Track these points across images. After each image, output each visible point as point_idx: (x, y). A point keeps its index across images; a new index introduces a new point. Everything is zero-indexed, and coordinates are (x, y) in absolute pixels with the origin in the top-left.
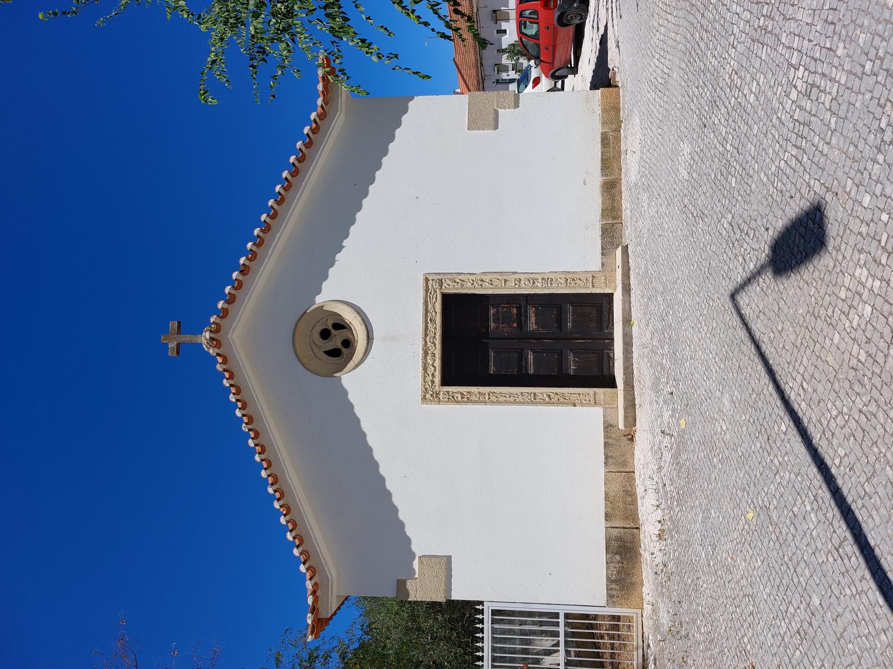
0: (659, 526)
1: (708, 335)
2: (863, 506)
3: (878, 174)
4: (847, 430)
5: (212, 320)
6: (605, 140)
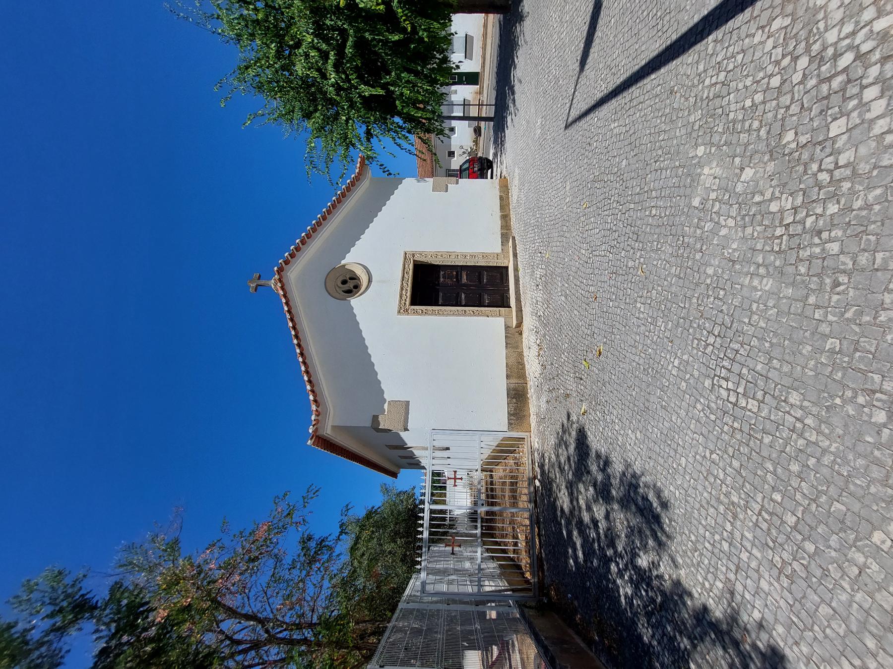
6: (501, 198)
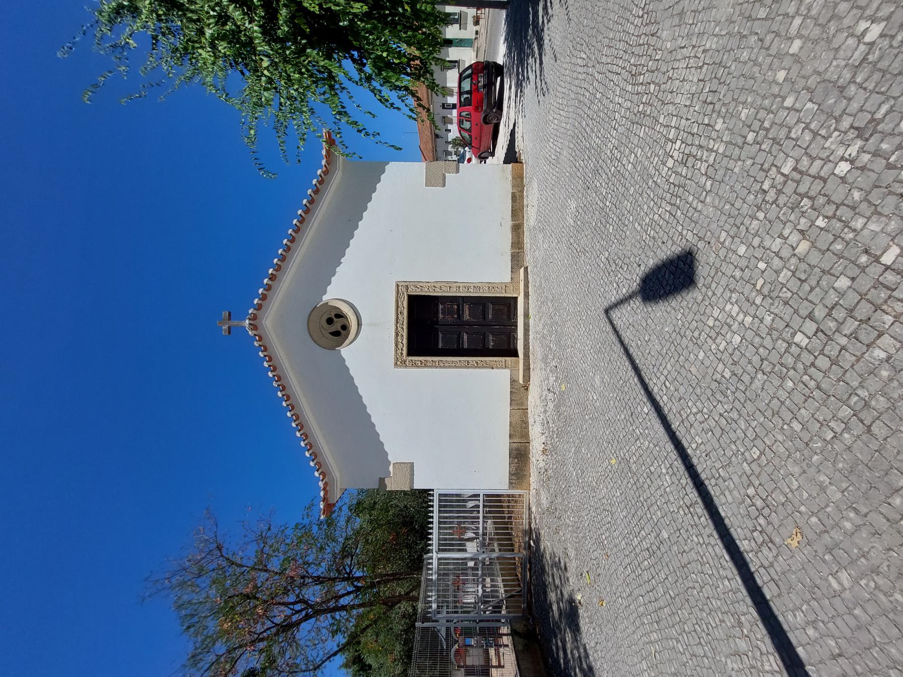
0: (543, 446)
1: (586, 333)
2: (716, 485)
3: (757, 228)
4: (705, 425)
5: (250, 312)
6: (514, 197)
